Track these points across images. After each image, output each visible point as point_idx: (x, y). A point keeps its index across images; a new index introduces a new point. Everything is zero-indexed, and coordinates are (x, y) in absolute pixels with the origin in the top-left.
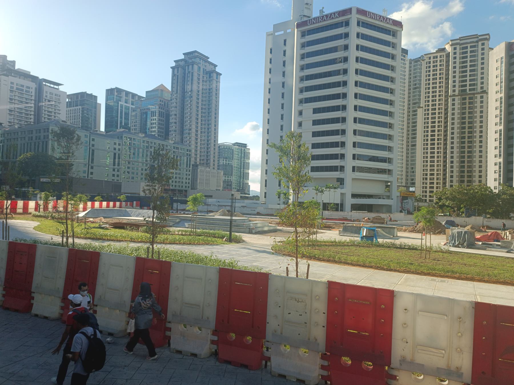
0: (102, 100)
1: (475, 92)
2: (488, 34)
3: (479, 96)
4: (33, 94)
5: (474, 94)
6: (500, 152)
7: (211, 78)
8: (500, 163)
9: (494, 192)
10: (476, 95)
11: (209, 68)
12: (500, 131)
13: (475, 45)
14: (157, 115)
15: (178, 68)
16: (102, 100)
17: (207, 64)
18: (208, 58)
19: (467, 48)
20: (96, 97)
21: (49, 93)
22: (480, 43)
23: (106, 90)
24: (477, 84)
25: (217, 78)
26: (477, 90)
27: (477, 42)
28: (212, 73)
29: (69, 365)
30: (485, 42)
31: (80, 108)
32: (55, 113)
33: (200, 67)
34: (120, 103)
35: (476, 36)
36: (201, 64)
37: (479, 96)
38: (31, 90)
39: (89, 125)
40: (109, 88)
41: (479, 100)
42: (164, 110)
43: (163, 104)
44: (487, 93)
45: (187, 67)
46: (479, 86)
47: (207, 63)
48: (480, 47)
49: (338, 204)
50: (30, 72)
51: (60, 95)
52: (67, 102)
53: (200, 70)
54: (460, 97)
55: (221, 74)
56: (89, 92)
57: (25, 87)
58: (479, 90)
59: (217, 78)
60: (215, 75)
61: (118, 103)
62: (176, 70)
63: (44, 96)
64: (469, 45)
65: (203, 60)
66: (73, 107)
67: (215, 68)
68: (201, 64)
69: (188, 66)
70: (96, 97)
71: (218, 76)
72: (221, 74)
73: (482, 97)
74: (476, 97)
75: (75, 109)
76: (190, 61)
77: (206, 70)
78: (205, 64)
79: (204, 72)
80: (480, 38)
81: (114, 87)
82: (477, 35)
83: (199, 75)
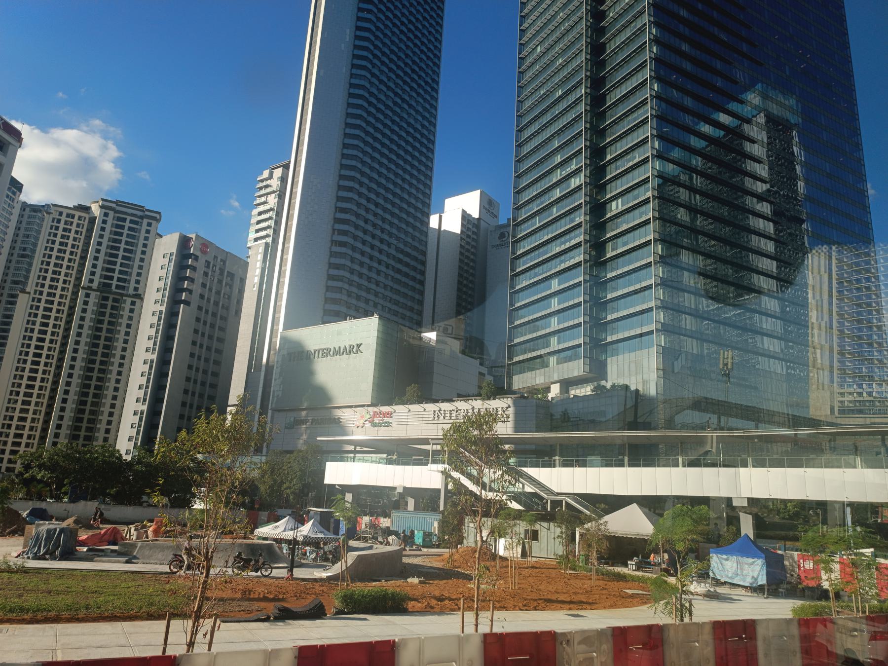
1: (124, 292)
2: (159, 213)
3: (129, 300)
5: (122, 295)
6: (145, 394)
8: (142, 412)
10: (124, 298)
12: (152, 361)
13: (138, 222)
19: (124, 220)
22: (145, 221)
24: (129, 281)
26: (128, 290)
27: (142, 217)
30: (154, 222)
35: (141, 208)
37: (129, 300)
41: (127, 306)
44: (142, 299)
46: (132, 285)
48: (145, 227)
49: (439, 491)
54: (99, 293)
58: (131, 291)
64: (129, 218)
73: (133, 303)
74: (125, 301)
80: (147, 213)
82: (143, 207)
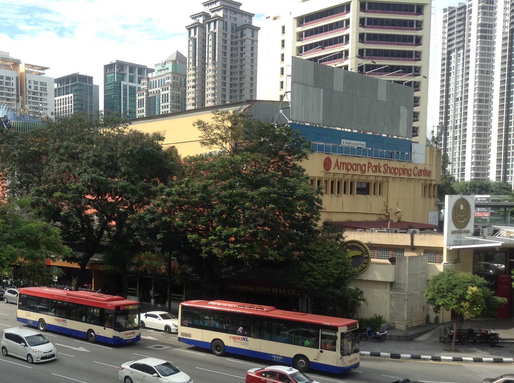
0: (99, 81)
4: (14, 87)
7: (244, 37)
9: (459, 297)
11: (241, 21)
14: (169, 100)
15: (195, 28)
16: (99, 81)
17: (238, 16)
18: (239, 4)
20: (91, 79)
21: (32, 82)
23: (104, 66)
25: (253, 36)
28: (245, 28)
29: (344, 366)
31: (71, 97)
32: (41, 94)
33: (226, 22)
34: (123, 83)
36: (229, 17)
38: (12, 81)
39: (84, 98)
40: (108, 63)
42: (179, 91)
43: (178, 82)
45: (207, 25)
47: (238, 14)
50: (8, 53)
51: (46, 83)
52: (55, 90)
53: (226, 28)
55: (259, 29)
56: (82, 73)
57: (4, 78)
59: (253, 36)
60: (248, 33)
61: (120, 84)
62: (193, 31)
63: (28, 87)
65: (231, 10)
66: (64, 95)
67: (251, 19)
68: (229, 17)
69: (209, 23)
70: (91, 79)
71: (255, 32)
72: (259, 29)
75: (66, 98)
76: (212, 15)
77: (236, 25)
78: (235, 16)
79: (232, 29)
81: (114, 61)
83: (226, 34)
